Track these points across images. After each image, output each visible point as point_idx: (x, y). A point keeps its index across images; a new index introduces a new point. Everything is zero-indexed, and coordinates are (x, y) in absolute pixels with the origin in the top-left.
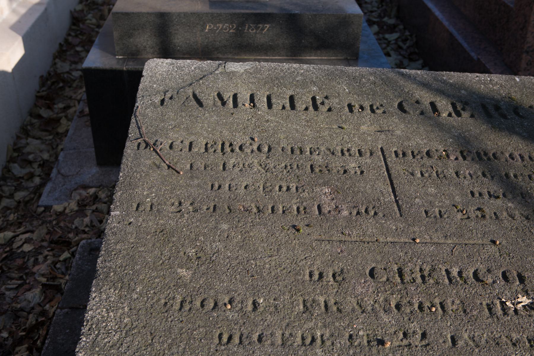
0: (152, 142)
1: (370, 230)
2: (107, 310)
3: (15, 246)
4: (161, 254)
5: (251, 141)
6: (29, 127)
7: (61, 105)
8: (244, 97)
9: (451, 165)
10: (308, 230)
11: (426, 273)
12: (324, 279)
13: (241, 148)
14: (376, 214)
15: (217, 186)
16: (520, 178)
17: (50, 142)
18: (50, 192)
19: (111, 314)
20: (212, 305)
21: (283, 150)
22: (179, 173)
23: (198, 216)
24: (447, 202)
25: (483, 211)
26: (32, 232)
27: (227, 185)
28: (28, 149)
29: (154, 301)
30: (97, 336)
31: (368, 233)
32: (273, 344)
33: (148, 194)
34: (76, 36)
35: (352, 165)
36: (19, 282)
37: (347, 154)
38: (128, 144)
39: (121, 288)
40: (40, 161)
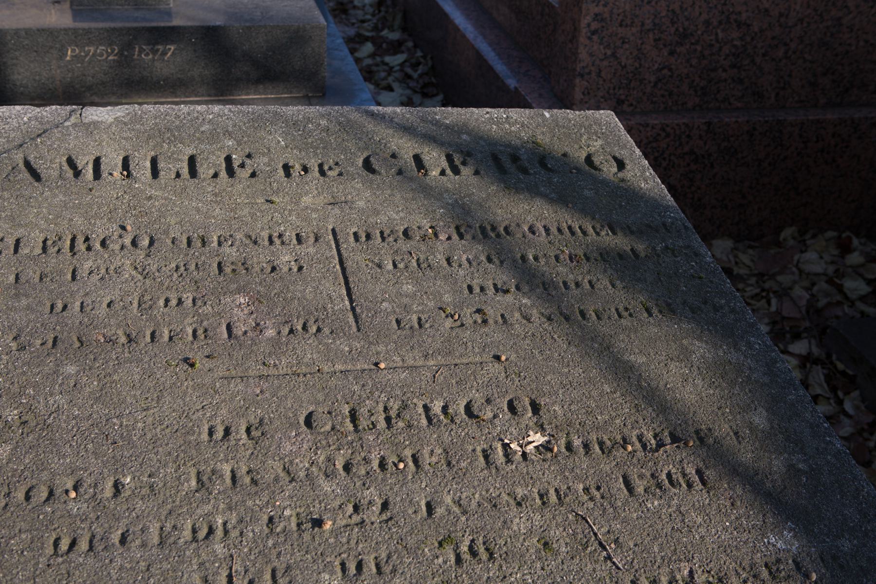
8: (113, 161)
35: (285, 259)
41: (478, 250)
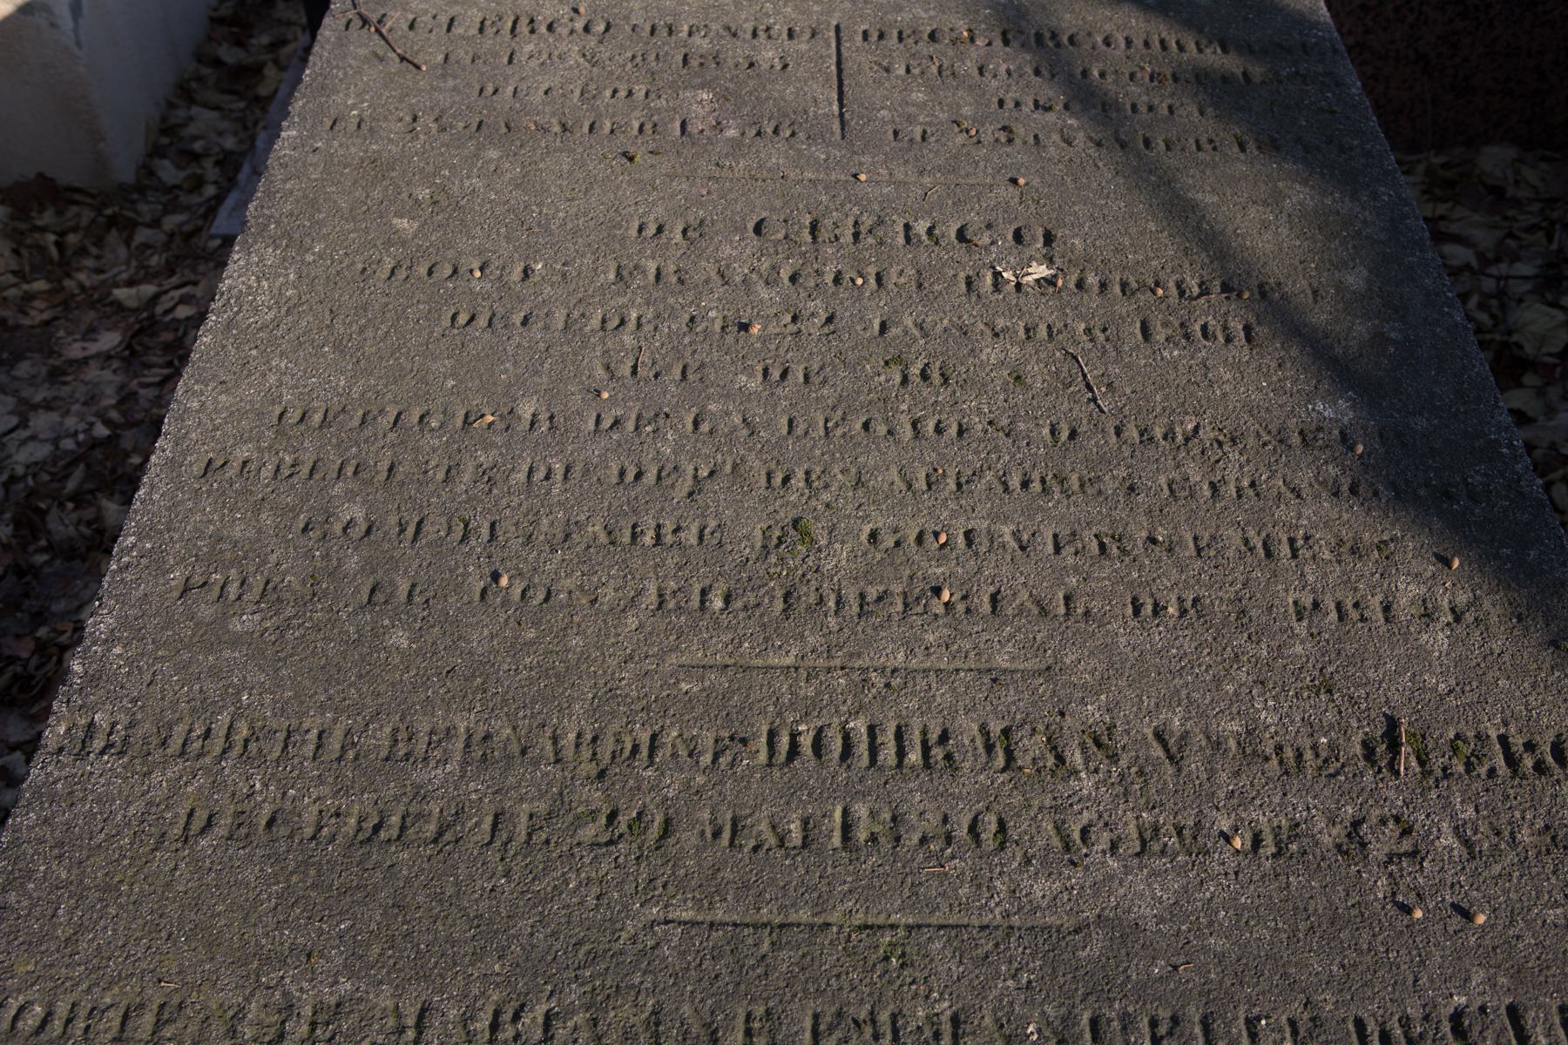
0: (374, 18)
1: (774, 160)
2: (258, 278)
3: (159, 310)
4: (367, 197)
5: (572, 14)
6: (194, 85)
7: (265, 40)
9: (974, 55)
10: (652, 160)
11: (863, 229)
12: (663, 236)
13: (550, 28)
14: (793, 134)
15: (490, 89)
16: (1110, 78)
17: (240, 115)
18: (234, 209)
19: (265, 284)
20: (449, 272)
21: (633, 30)
22: (418, 67)
23: (446, 137)
24: (943, 116)
25: (1011, 131)
26: (195, 283)
27: (511, 89)
28: (192, 130)
29: (344, 265)
30: (237, 313)
31: (769, 165)
32: (546, 328)
33: (354, 104)
35: (768, 55)
36: (166, 371)
37: (762, 35)
38: (327, 20)
39: (287, 246)
40: (218, 154)
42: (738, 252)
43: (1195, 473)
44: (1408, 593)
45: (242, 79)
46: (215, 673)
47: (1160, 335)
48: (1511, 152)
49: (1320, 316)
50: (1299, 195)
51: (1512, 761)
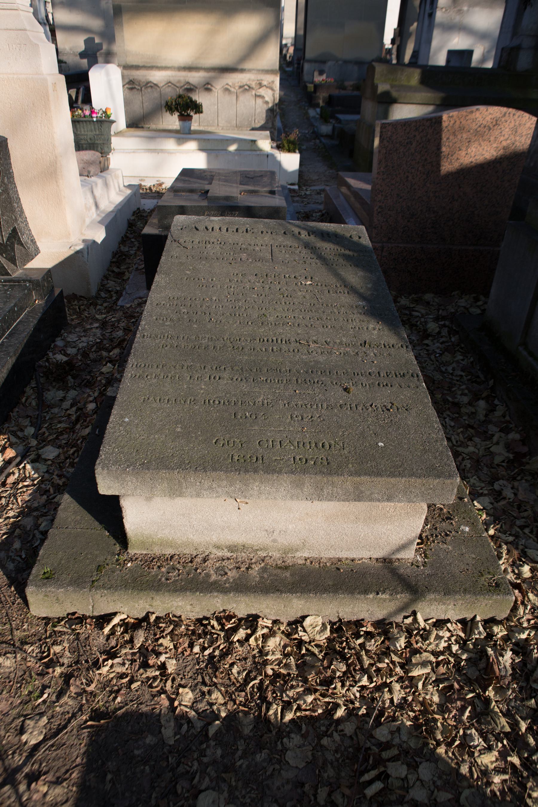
3: (107, 319)
8: (217, 227)
28: (108, 286)
34: (131, 234)
35: (257, 248)
41: (309, 251)
42: (253, 278)
43: (335, 310)
44: (371, 326)
45: (120, 275)
46: (164, 329)
47: (331, 292)
48: (432, 295)
49: (362, 291)
50: (361, 273)
51: (385, 346)
